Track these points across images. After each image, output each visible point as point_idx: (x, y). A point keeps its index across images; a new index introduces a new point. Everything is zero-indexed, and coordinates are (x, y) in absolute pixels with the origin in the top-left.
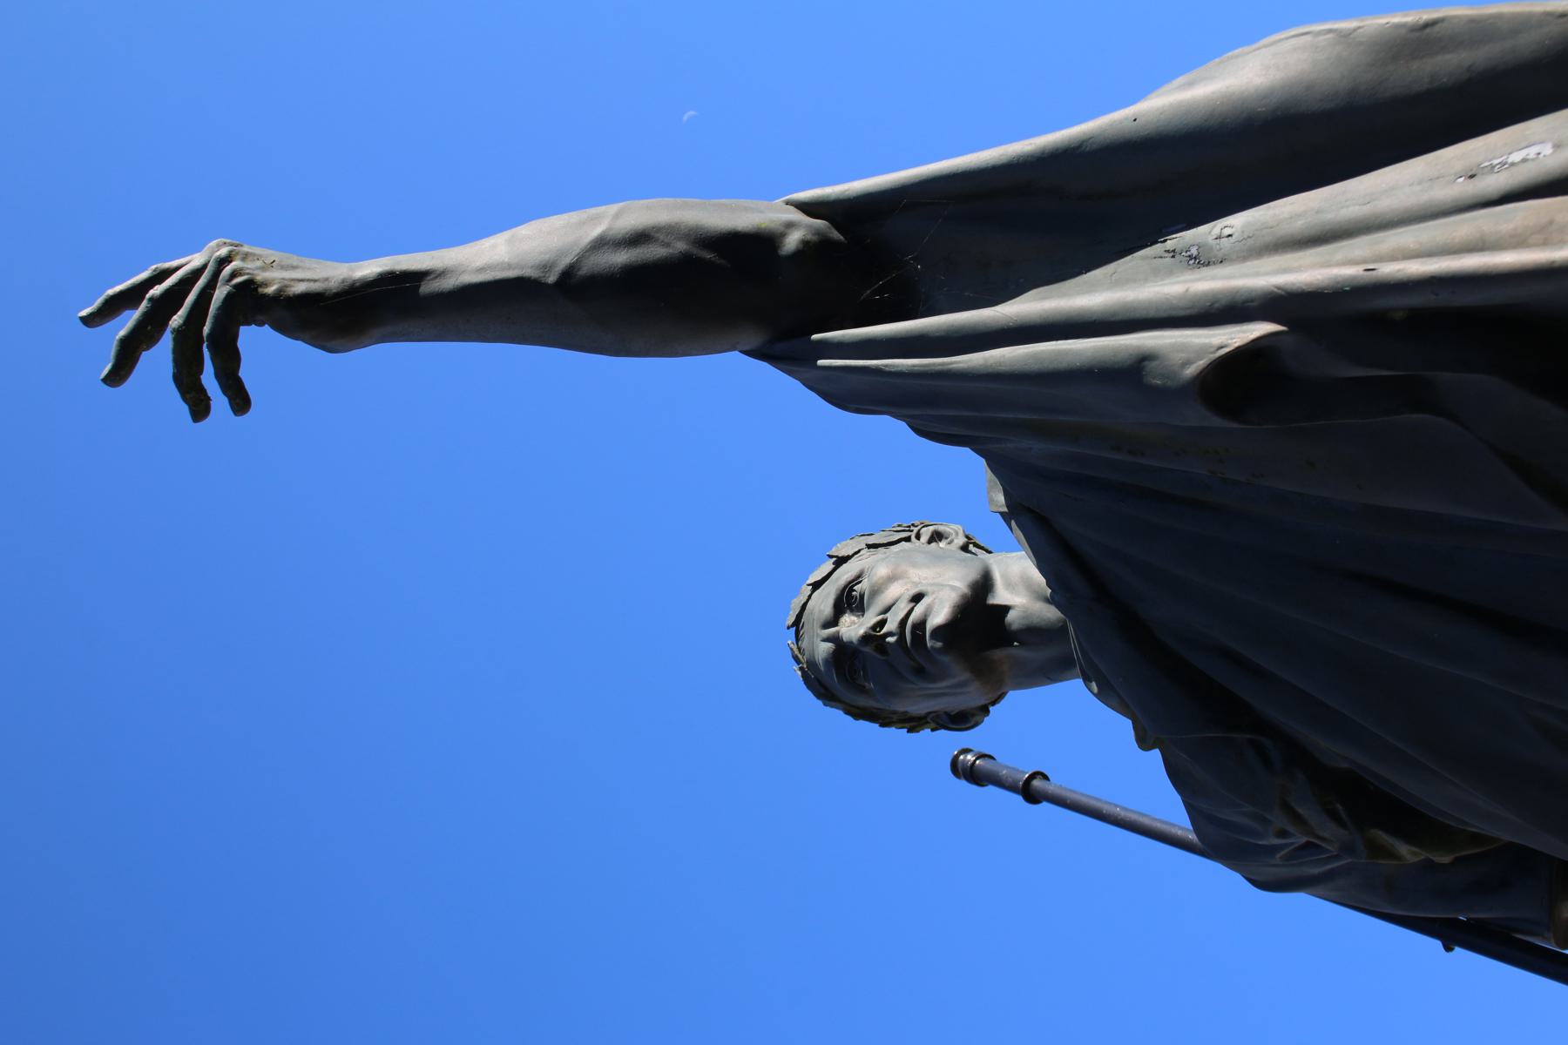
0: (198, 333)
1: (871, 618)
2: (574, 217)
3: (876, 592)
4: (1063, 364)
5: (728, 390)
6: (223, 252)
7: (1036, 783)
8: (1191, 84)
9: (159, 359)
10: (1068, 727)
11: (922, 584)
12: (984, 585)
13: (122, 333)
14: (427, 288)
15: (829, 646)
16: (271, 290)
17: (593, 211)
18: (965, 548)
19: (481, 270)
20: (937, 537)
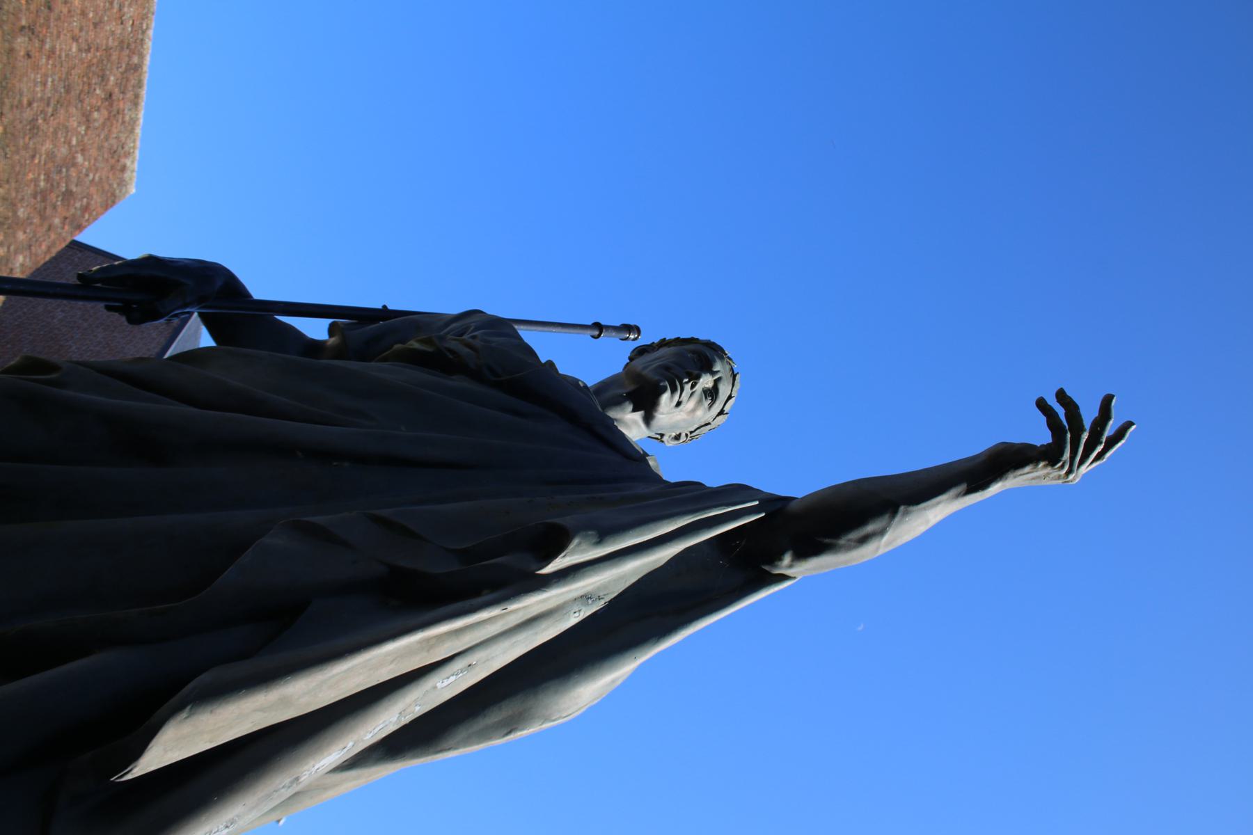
0: (1072, 433)
1: (699, 388)
2: (899, 542)
3: (700, 401)
4: (638, 530)
5: (799, 479)
6: (1071, 477)
7: (597, 333)
8: (613, 681)
9: (1089, 415)
10: (588, 363)
11: (678, 412)
12: (648, 419)
13: (1111, 422)
14: (963, 487)
15: (715, 369)
16: (1041, 464)
17: (891, 548)
18: (662, 435)
19: (938, 503)
20: (677, 437)
